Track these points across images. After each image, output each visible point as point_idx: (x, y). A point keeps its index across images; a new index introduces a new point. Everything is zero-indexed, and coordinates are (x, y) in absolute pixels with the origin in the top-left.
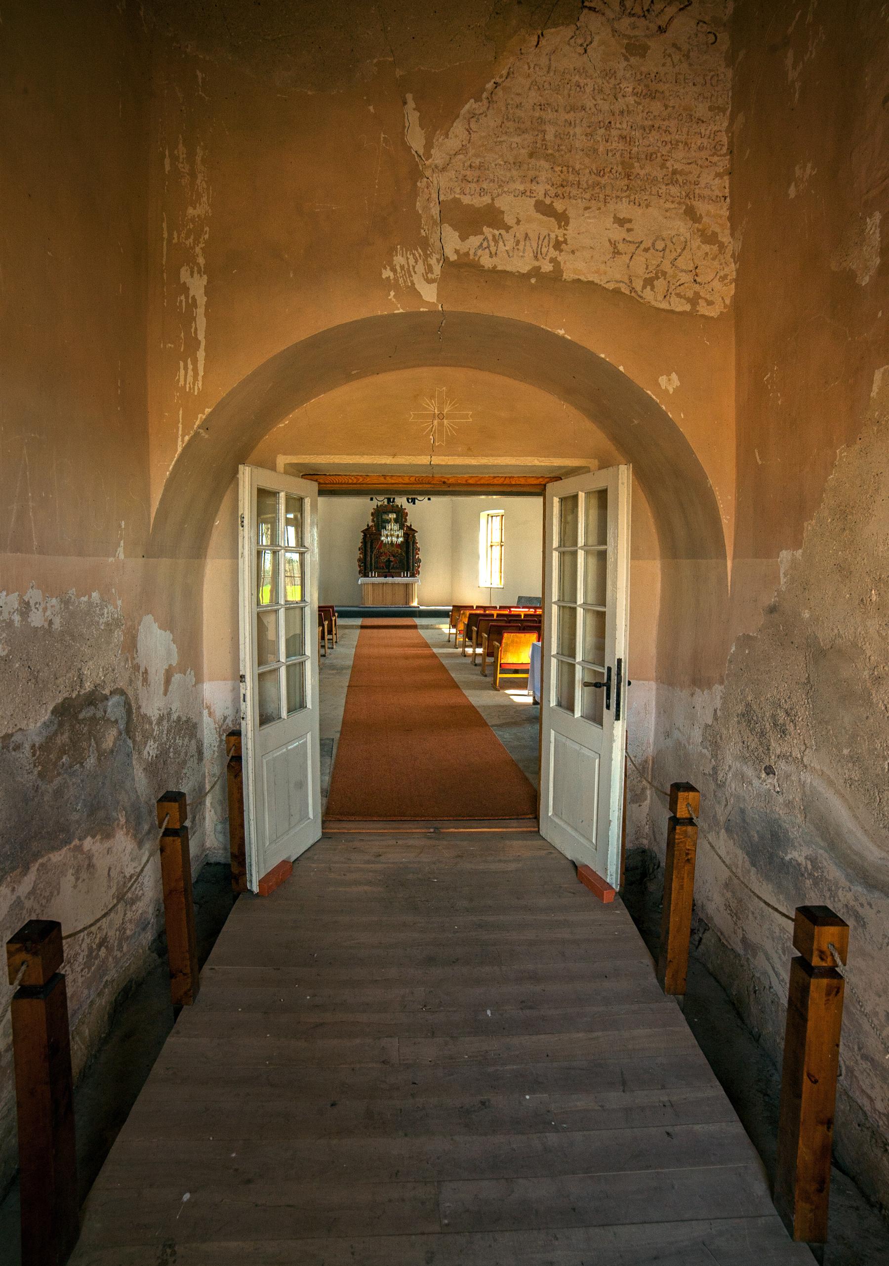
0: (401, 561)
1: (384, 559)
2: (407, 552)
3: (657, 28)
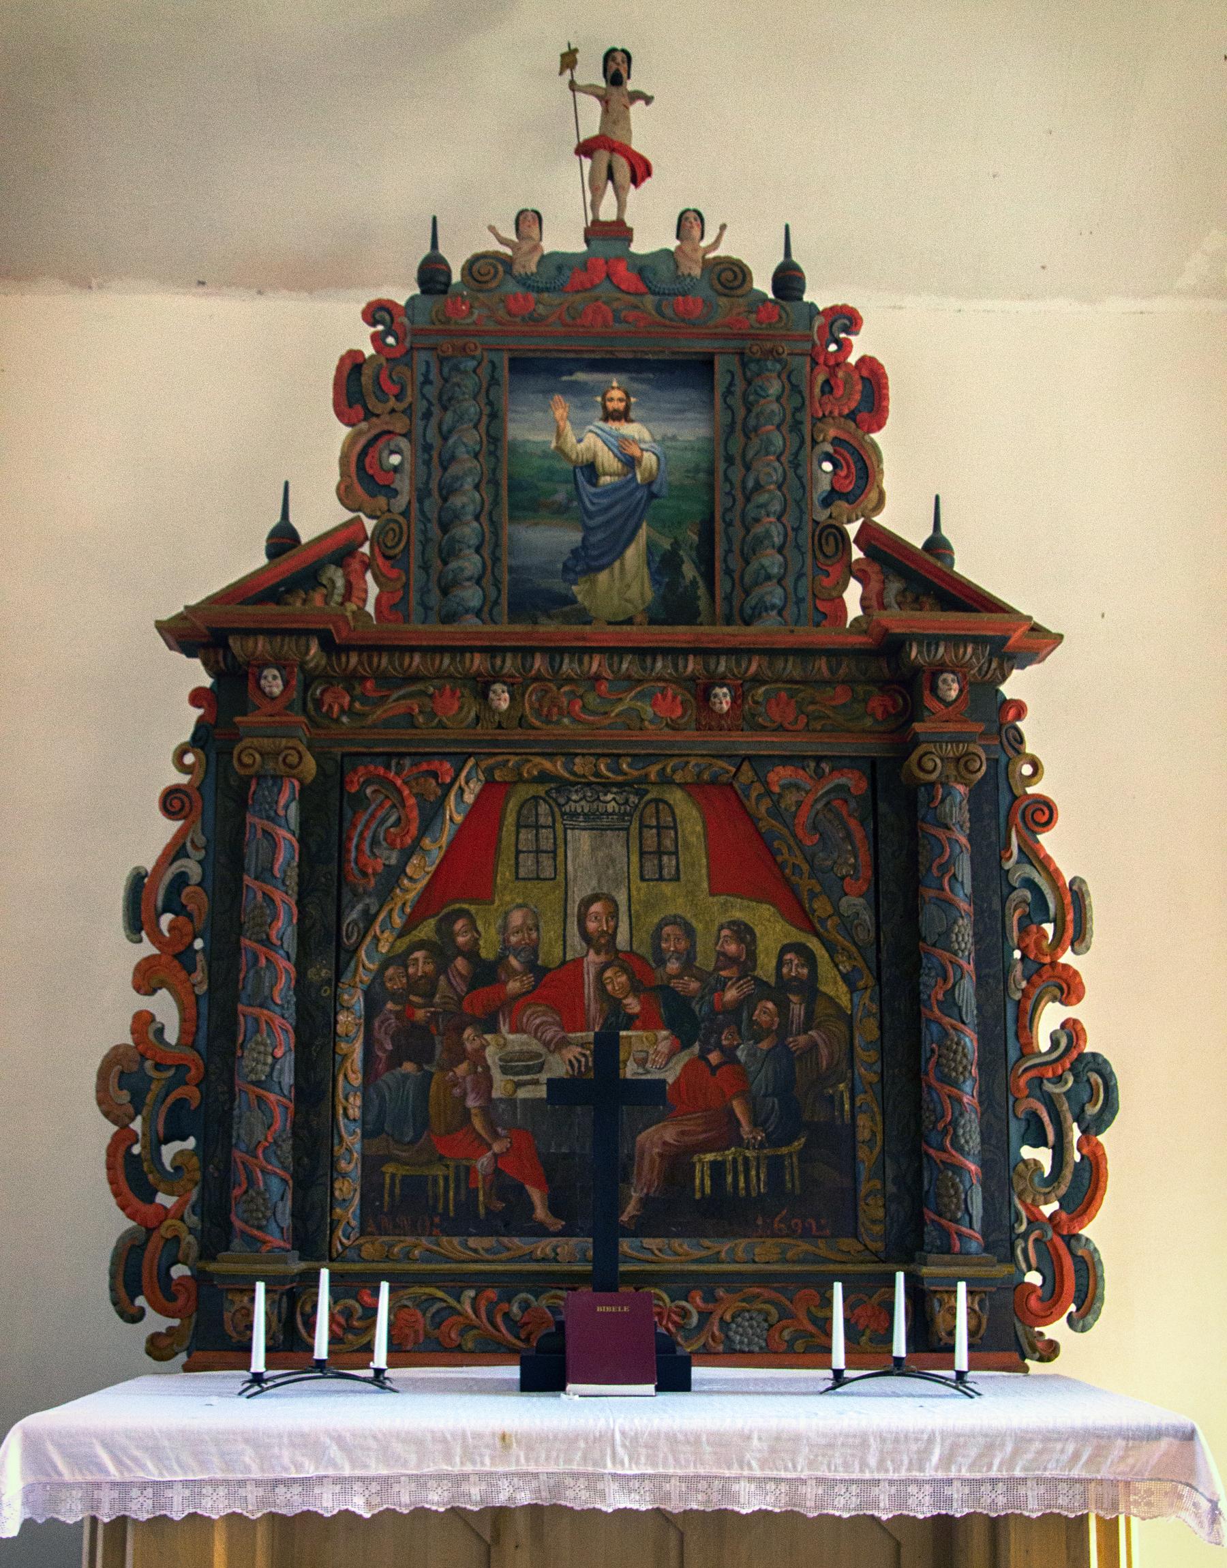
0: (793, 1107)
1: (520, 1061)
2: (900, 963)
3: (519, 1550)
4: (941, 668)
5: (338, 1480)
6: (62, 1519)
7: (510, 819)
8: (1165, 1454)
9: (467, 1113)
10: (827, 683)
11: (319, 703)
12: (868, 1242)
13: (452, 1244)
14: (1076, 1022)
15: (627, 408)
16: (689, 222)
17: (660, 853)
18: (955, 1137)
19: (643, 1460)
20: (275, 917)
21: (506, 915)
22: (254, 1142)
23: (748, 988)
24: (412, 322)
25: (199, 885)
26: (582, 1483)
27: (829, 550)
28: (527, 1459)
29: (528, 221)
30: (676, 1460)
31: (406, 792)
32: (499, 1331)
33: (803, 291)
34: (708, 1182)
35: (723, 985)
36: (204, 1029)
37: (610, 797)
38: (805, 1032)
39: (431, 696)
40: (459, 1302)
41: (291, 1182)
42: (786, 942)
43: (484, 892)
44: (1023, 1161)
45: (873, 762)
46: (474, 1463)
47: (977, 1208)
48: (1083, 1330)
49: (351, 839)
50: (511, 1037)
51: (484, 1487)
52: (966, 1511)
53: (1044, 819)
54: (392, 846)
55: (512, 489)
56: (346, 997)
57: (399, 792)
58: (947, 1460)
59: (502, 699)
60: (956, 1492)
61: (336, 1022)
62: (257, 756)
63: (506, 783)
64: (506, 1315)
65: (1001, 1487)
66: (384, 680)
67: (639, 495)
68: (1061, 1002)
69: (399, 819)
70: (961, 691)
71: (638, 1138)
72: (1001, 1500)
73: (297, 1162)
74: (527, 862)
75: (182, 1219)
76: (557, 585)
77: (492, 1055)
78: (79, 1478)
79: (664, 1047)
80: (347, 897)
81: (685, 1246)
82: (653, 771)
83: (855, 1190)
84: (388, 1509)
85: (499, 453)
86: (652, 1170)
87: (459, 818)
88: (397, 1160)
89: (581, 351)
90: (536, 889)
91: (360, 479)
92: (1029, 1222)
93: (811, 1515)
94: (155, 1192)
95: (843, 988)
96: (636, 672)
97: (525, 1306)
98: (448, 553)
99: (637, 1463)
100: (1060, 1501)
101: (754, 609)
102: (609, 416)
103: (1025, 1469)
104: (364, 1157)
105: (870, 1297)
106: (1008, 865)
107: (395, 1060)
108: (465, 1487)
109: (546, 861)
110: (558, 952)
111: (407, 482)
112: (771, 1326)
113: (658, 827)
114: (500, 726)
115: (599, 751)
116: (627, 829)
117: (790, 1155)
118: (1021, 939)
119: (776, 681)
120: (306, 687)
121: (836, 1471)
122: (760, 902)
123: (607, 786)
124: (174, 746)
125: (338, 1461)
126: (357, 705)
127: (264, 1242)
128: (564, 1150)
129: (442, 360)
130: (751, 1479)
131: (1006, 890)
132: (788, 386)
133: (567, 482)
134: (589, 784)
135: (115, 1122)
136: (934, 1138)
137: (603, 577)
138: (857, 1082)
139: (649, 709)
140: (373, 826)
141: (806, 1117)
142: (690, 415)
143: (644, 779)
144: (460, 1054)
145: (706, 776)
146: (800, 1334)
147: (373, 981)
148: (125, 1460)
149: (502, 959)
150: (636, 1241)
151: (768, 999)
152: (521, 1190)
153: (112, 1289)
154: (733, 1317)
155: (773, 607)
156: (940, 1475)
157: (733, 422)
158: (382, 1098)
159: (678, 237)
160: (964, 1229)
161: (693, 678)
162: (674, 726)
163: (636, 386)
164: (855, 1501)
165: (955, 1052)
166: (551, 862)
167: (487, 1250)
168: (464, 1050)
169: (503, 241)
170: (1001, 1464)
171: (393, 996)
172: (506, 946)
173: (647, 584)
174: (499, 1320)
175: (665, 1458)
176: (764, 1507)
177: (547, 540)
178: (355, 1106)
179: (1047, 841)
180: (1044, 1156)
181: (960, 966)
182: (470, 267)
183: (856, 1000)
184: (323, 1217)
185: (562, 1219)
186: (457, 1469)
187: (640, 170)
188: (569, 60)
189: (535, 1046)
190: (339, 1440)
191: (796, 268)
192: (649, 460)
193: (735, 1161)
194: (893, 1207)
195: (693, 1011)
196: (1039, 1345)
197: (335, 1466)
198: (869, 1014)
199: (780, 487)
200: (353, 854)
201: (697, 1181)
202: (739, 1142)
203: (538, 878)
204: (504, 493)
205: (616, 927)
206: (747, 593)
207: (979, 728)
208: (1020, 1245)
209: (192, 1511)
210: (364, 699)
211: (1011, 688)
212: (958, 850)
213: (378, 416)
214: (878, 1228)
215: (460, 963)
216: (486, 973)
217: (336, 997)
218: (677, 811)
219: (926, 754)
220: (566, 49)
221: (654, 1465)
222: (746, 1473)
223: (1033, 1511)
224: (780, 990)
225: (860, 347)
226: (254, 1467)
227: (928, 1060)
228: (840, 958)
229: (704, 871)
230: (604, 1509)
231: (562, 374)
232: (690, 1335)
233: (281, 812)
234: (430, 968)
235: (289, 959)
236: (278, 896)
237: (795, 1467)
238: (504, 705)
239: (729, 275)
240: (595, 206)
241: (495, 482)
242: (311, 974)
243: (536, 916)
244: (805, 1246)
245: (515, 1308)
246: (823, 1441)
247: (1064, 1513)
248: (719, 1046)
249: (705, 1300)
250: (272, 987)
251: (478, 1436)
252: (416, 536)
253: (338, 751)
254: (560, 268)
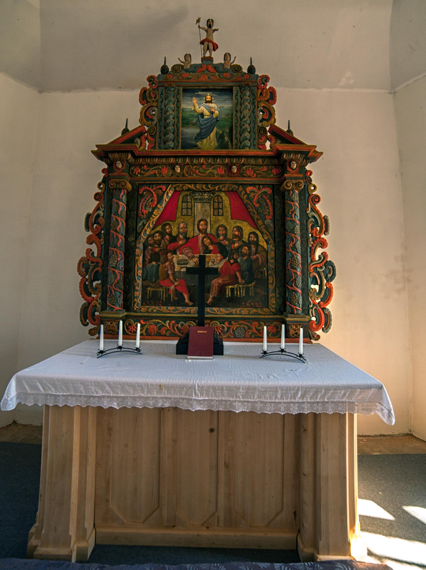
1: (181, 261)
4: (292, 160)
5: (109, 397)
6: (27, 404)
7: (180, 200)
8: (373, 394)
9: (168, 274)
10: (261, 165)
11: (132, 171)
12: (271, 309)
13: (164, 308)
14: (325, 253)
15: (211, 100)
16: (227, 56)
17: (218, 209)
18: (295, 283)
19: (205, 395)
20: (118, 224)
21: (179, 224)
22: (112, 282)
23: (241, 243)
24: (158, 80)
25: (103, 217)
26: (185, 401)
27: (262, 133)
28: (168, 393)
29: (188, 56)
30: (215, 395)
31: (154, 193)
32: (175, 331)
33: (255, 72)
34: (230, 293)
35: (234, 243)
36: (103, 254)
37: (206, 194)
38: (256, 255)
39: (161, 169)
40: (165, 323)
41: (122, 293)
42: (251, 231)
43: (173, 219)
44: (312, 289)
45: (273, 185)
46: (151, 394)
47: (301, 303)
48: (326, 332)
49: (140, 205)
50: (180, 255)
51: (154, 401)
52: (309, 412)
53: (317, 200)
54: (150, 207)
55: (182, 119)
56: (138, 245)
57: (152, 193)
58: (303, 396)
59: (178, 170)
61: (135, 251)
62: (115, 184)
63: (179, 191)
64: (177, 327)
65: (320, 404)
66: (149, 165)
67: (214, 120)
68: (322, 248)
69: (152, 200)
70: (297, 166)
71: (212, 282)
72: (320, 408)
73: (125, 287)
74: (185, 211)
75: (97, 301)
76: (194, 142)
77: (175, 260)
78: (32, 392)
79: (219, 258)
80: (139, 220)
81: (224, 310)
82: (217, 188)
83: (268, 296)
84: (124, 407)
85: (179, 110)
86: (215, 290)
87: (167, 200)
88: (151, 286)
89: (200, 86)
90: (187, 218)
91: (145, 118)
92: (313, 305)
93: (259, 413)
94: (91, 294)
95: (265, 243)
96: (213, 163)
97: (182, 325)
98: (166, 134)
99: (203, 396)
100: (339, 409)
101: (243, 147)
102: (207, 102)
103: (328, 399)
104: (143, 286)
105: (272, 324)
106: (308, 212)
107: (150, 261)
108: (148, 401)
109: (189, 211)
110: (192, 233)
111: (156, 118)
112: (246, 331)
113: (218, 202)
114: (178, 176)
115: (203, 182)
116: (210, 203)
117: (251, 286)
118: (311, 231)
119: (248, 165)
120: (130, 167)
121: (267, 399)
122: (244, 221)
123: (205, 192)
124: (98, 183)
125: (109, 391)
126: (142, 172)
127: (114, 308)
128: (193, 285)
129: (166, 88)
130: (239, 401)
131: (307, 219)
132: (251, 94)
133: (196, 118)
134: (201, 191)
135: (82, 276)
136: (289, 283)
137: (205, 140)
138: (269, 267)
139: (216, 172)
140: (145, 202)
141: (255, 277)
142: (227, 101)
143: (214, 190)
144: (166, 260)
145: (230, 189)
146: (253, 333)
147: (145, 241)
148: (45, 387)
149: (178, 235)
150: (211, 308)
151: (246, 246)
152: (182, 294)
153: (81, 317)
154: (236, 329)
155: (248, 146)
156: (301, 401)
157: (238, 102)
158: (147, 271)
159: (224, 60)
160: (298, 308)
161: (227, 164)
162: (222, 176)
163: (214, 95)
164: (273, 409)
165: (296, 261)
166: (190, 211)
167: (173, 310)
168: (168, 259)
169: (182, 62)
170: (320, 397)
171: (150, 245)
172: (179, 232)
173: (216, 142)
174: (175, 328)
175: (212, 394)
176: (243, 410)
178: (140, 272)
179: (318, 206)
180: (317, 287)
181: (297, 238)
182: (173, 68)
183: (269, 246)
184: (131, 302)
185: (192, 302)
186: (145, 396)
187: (216, 47)
188: (198, 21)
189: (186, 258)
190: (109, 384)
191: (253, 66)
192: (217, 112)
193: (237, 288)
194: (278, 300)
195: (226, 249)
196: (315, 336)
197: (108, 393)
198: (272, 250)
199: (249, 118)
200: (140, 209)
201: (227, 293)
202: (238, 283)
203: (187, 215)
204: (181, 120)
205: (207, 227)
206: (241, 143)
207: (301, 176)
208: (311, 310)
209: (65, 404)
210: (144, 170)
211: (308, 168)
212: (296, 207)
213: (150, 102)
214: (274, 306)
215: (167, 237)
216: (174, 239)
217: (135, 245)
218: (223, 199)
219: (288, 182)
220: (197, 19)
221: (208, 396)
222: (238, 399)
223: (330, 412)
224: (249, 244)
226: (83, 391)
227: (288, 263)
228: (265, 236)
229: (230, 213)
230: (192, 410)
231: (195, 92)
232: (225, 333)
233: (121, 198)
234: (160, 238)
235: (122, 235)
236: (119, 219)
237: (254, 398)
238: (179, 171)
239: (237, 68)
240: (204, 54)
241: (178, 117)
242: (129, 239)
243: (187, 225)
244: (255, 310)
245: (180, 326)
246: (263, 390)
247: (340, 413)
248: (233, 258)
249: (229, 324)
250: (117, 242)
251: (152, 385)
252: (158, 130)
253: (137, 183)
254: (195, 67)
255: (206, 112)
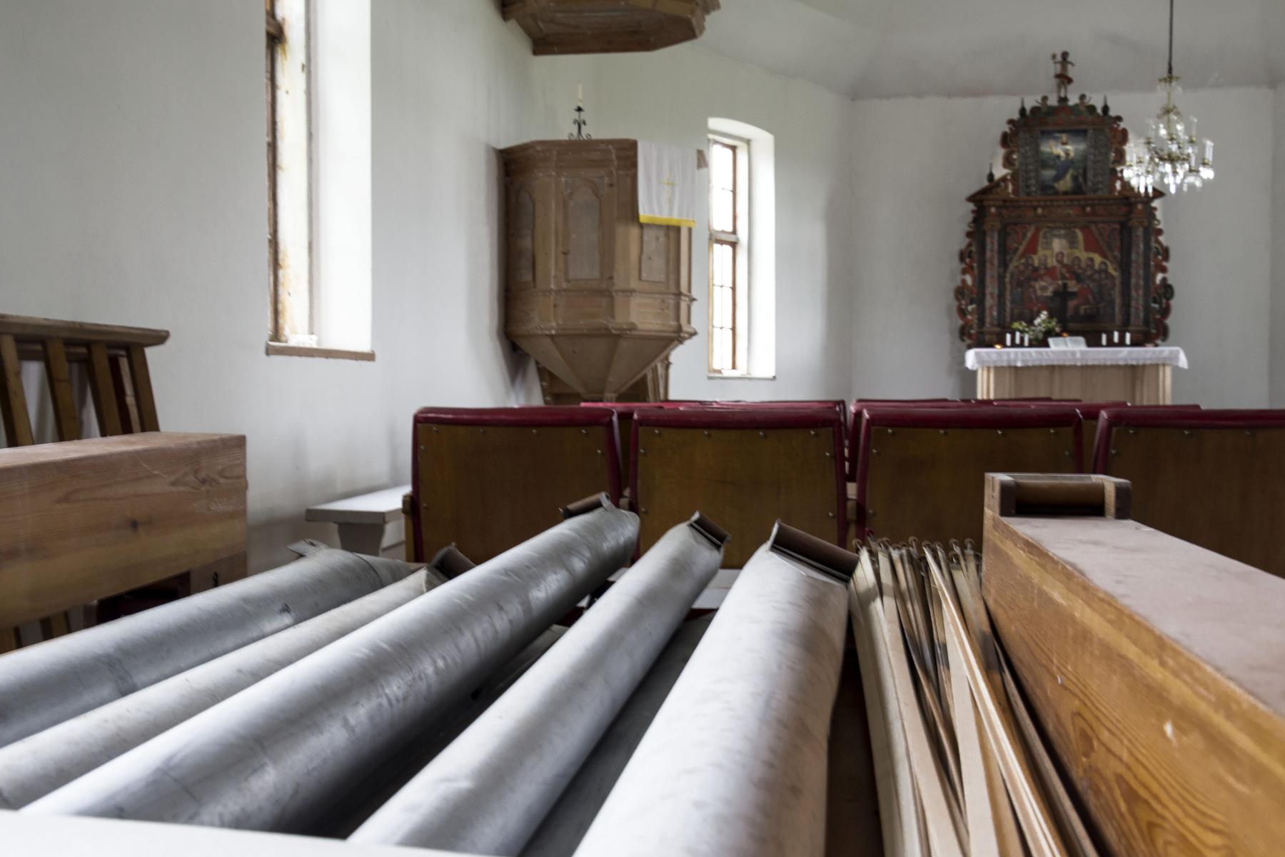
1: (1044, 288)
16: (1083, 97)
29: (1045, 98)
43: (1035, 252)
60: (1078, 356)
177: (1049, 174)
179: (1161, 238)
216: (1036, 269)
224: (1099, 272)
225: (1122, 125)
255: (1062, 154)
